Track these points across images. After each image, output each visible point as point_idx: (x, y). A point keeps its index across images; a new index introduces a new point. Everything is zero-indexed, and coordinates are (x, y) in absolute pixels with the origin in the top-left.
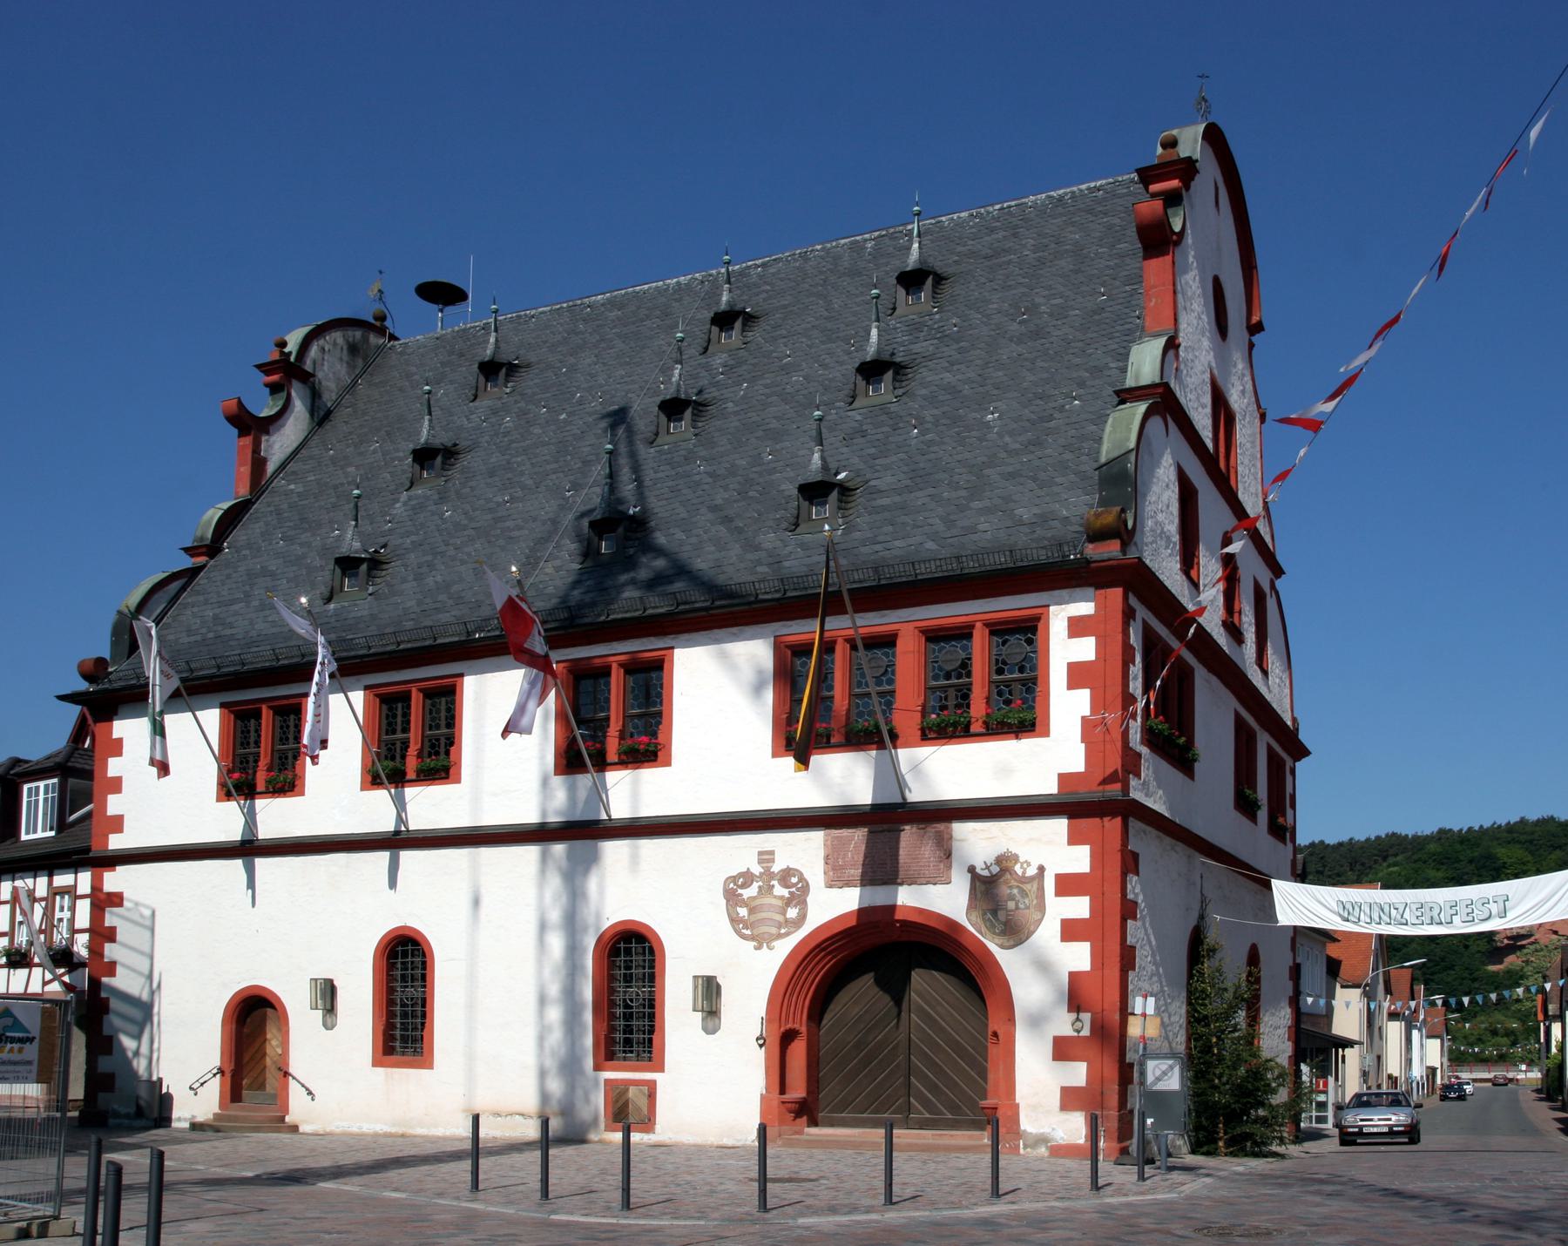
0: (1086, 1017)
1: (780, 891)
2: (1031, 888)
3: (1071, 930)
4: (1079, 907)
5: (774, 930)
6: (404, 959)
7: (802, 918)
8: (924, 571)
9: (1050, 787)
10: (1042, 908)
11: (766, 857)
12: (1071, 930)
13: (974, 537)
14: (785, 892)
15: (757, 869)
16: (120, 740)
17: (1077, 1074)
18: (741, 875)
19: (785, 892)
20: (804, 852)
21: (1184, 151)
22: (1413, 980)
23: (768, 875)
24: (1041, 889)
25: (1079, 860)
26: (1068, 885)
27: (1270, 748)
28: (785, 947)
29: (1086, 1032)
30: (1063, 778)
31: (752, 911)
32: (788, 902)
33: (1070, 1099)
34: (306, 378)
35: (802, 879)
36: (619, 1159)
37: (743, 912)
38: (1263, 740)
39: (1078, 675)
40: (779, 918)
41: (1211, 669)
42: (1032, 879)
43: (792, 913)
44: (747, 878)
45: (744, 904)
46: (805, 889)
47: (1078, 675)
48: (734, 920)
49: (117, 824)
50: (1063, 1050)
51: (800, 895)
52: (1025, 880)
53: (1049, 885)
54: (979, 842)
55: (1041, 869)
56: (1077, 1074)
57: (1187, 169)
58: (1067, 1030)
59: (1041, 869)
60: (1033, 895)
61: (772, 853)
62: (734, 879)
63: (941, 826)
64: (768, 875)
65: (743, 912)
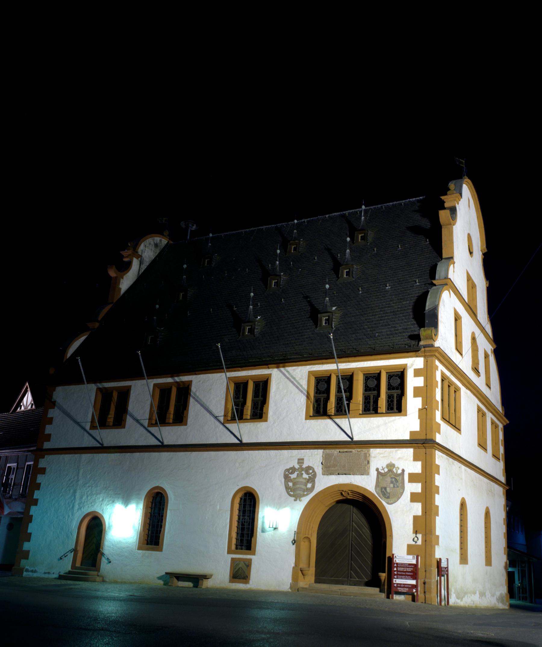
0: (420, 536)
1: (305, 476)
3: (414, 498)
4: (417, 488)
5: (302, 493)
9: (407, 437)
10: (403, 488)
11: (301, 461)
12: (414, 498)
15: (297, 466)
18: (291, 468)
20: (314, 458)
23: (301, 469)
25: (417, 467)
27: (492, 419)
28: (306, 500)
29: (419, 542)
30: (412, 433)
35: (314, 471)
37: (291, 484)
39: (417, 392)
40: (304, 487)
42: (400, 475)
43: (309, 485)
44: (293, 470)
45: (291, 480)
46: (315, 475)
47: (417, 392)
48: (287, 488)
51: (312, 479)
54: (379, 459)
55: (403, 471)
59: (403, 471)
60: (400, 482)
61: (303, 459)
62: (287, 470)
63: (365, 450)
64: (301, 469)
65: (291, 484)
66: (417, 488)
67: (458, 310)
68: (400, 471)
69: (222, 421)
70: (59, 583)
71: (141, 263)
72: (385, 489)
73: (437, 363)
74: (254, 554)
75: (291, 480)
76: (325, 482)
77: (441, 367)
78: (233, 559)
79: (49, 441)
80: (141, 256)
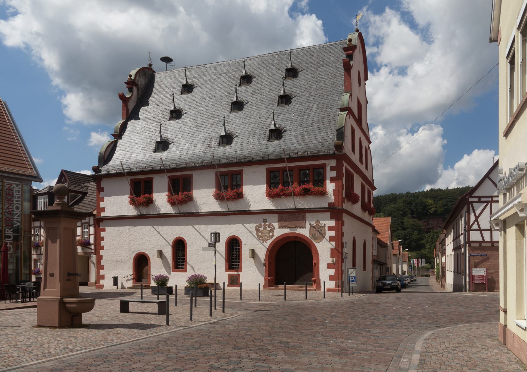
0: (334, 259)
1: (268, 229)
2: (323, 229)
3: (331, 239)
4: (333, 234)
6: (179, 246)
7: (272, 236)
8: (300, 155)
12: (331, 239)
13: (310, 145)
14: (269, 229)
16: (103, 188)
17: (332, 272)
19: (269, 229)
21: (353, 43)
22: (399, 245)
24: (325, 229)
26: (330, 228)
28: (269, 242)
31: (262, 233)
32: (270, 231)
33: (331, 278)
34: (136, 85)
36: (258, 293)
37: (260, 234)
38: (367, 187)
41: (357, 173)
43: (271, 234)
45: (260, 232)
46: (274, 228)
47: (332, 180)
49: (103, 210)
50: (329, 266)
51: (272, 230)
52: (321, 227)
53: (326, 228)
54: (310, 221)
55: (325, 224)
56: (332, 272)
57: (354, 48)
58: (331, 262)
59: (325, 224)
66: (333, 234)
67: (361, 101)
68: (323, 225)
69: (131, 211)
70: (292, 207)
71: (138, 90)
72: (315, 235)
73: (344, 162)
74: (241, 271)
75: (260, 232)
76: (279, 232)
77: (345, 164)
78: (230, 276)
79: (104, 211)
80: (138, 85)
